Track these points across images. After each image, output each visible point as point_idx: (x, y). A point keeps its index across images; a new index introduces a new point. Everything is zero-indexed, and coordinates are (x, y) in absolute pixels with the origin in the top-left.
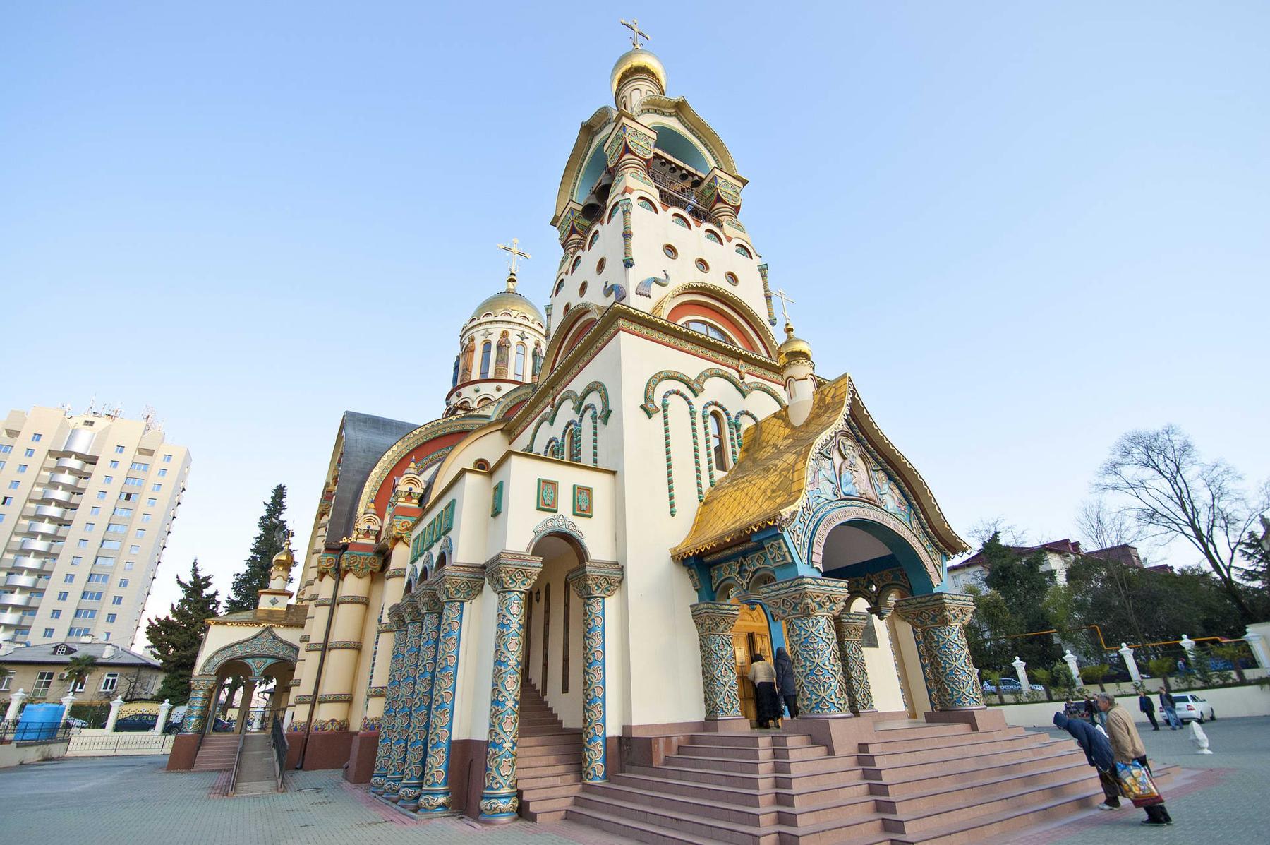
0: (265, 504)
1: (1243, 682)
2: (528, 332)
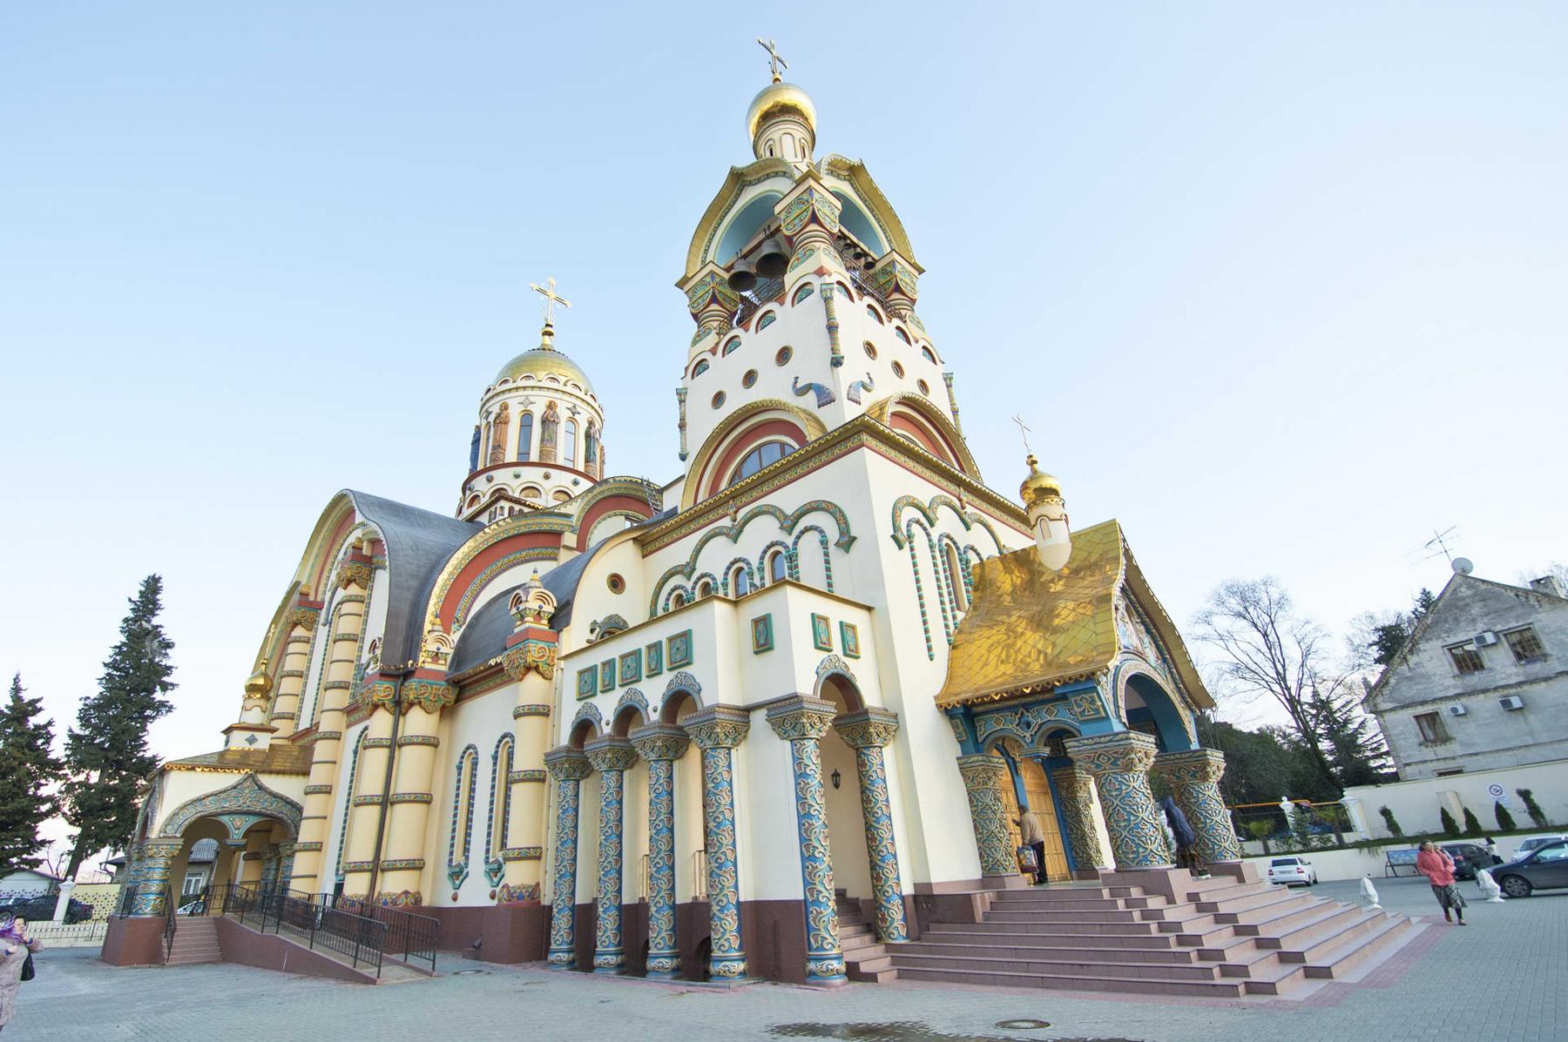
0: (130, 600)
1: (1342, 846)
2: (581, 406)
